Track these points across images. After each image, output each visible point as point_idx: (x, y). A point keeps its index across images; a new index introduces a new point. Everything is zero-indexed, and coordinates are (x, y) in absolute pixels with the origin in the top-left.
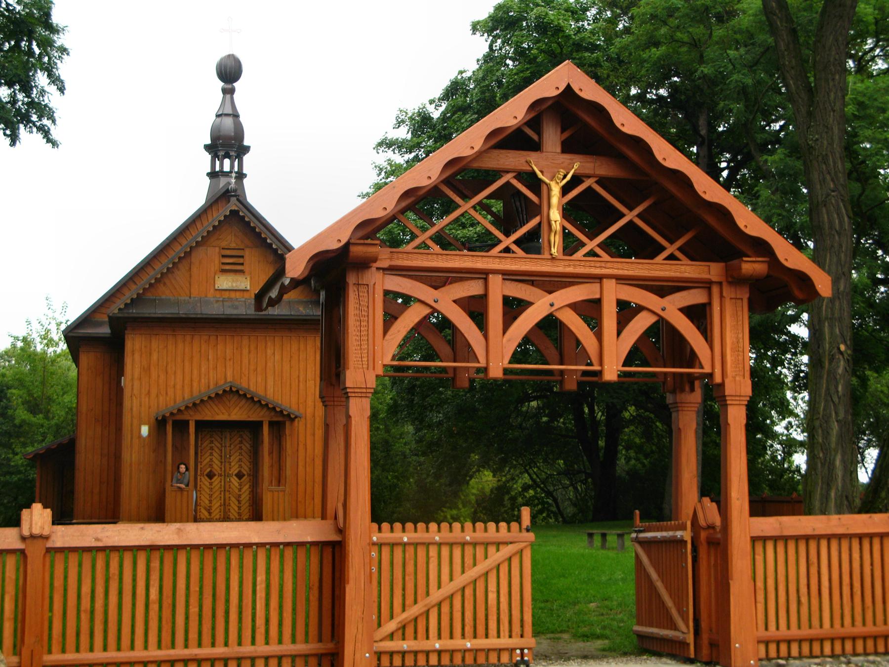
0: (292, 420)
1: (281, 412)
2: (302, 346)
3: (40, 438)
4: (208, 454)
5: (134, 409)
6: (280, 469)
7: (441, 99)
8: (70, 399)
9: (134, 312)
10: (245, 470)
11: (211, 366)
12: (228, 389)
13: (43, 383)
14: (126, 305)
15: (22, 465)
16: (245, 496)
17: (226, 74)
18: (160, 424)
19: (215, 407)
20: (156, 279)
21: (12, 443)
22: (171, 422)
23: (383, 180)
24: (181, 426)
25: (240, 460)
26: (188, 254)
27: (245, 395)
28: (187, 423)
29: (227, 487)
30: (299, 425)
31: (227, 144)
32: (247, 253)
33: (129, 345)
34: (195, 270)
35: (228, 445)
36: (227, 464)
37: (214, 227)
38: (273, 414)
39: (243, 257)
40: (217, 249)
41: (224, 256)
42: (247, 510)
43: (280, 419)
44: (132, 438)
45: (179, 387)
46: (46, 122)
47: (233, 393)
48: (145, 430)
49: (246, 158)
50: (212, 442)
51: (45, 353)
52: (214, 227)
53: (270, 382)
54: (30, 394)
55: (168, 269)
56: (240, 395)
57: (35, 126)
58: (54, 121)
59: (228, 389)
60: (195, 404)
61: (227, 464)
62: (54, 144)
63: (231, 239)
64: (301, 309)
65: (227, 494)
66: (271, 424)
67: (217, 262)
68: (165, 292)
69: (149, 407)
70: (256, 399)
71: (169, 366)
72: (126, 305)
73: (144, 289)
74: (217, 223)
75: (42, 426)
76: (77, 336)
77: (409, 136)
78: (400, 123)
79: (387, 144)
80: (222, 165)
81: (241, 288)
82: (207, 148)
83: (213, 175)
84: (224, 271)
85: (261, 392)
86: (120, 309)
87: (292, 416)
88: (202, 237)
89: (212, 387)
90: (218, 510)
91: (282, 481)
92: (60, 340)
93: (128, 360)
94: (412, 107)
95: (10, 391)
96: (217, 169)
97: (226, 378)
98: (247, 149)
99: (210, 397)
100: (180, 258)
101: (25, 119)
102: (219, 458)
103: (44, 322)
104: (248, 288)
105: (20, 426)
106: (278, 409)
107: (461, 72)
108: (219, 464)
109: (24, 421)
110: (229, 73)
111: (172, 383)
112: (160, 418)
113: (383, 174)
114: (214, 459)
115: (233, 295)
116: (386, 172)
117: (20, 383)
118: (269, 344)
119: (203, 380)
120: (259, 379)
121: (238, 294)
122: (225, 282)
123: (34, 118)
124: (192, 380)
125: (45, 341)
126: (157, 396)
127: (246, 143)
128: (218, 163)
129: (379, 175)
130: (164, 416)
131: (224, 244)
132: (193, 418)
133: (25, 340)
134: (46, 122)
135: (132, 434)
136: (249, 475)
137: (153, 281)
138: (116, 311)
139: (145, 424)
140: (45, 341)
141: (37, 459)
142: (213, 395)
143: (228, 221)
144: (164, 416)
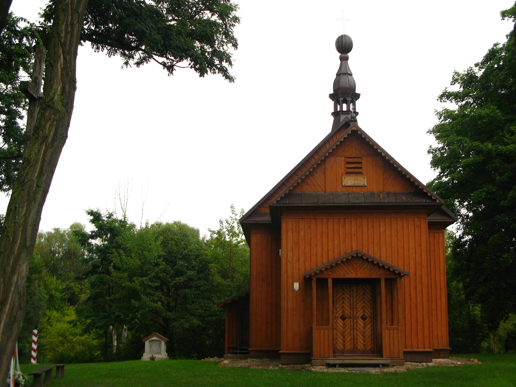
0: (401, 277)
1: (394, 271)
2: (405, 224)
3: (229, 294)
4: (341, 302)
5: (289, 271)
6: (392, 313)
7: (483, 63)
8: (245, 269)
9: (287, 203)
10: (368, 314)
11: (341, 240)
12: (355, 255)
13: (230, 259)
14: (282, 198)
15: (218, 311)
16: (368, 333)
17: (342, 47)
18: (307, 281)
19: (345, 268)
20: (302, 179)
21: (212, 297)
22: (315, 280)
23: (443, 122)
24: (322, 283)
25: (364, 307)
26: (323, 162)
27: (367, 259)
28: (326, 280)
29: (335, 326)
30: (405, 281)
31: (344, 92)
32: (364, 160)
33: (284, 226)
34: (328, 173)
35: (355, 296)
36: (355, 310)
37: (341, 142)
38: (387, 273)
39: (361, 163)
40: (343, 158)
41: (348, 163)
42: (370, 343)
43: (393, 277)
44: (287, 292)
45: (319, 255)
46: (225, 64)
47: (357, 258)
48: (296, 286)
49: (358, 102)
50: (343, 294)
51: (231, 241)
52: (341, 142)
53: (383, 249)
54: (222, 267)
55: (310, 172)
56: (364, 260)
57: (217, 68)
58: (230, 64)
59: (355, 255)
60: (332, 267)
61: (355, 310)
62: (231, 79)
63: (353, 150)
64: (404, 198)
65: (355, 331)
66: (387, 280)
67: (343, 167)
68: (308, 189)
69: (299, 270)
70: (375, 262)
71: (312, 240)
72: (282, 198)
73: (294, 187)
74: (342, 140)
75: (230, 286)
76: (249, 222)
77: (462, 89)
78: (454, 81)
79: (446, 96)
80: (341, 107)
81: (360, 185)
82: (332, 96)
83: (336, 114)
84: (348, 173)
85: (377, 256)
86: (277, 201)
87: (402, 274)
88: (333, 149)
89: (342, 254)
90: (349, 343)
91: (395, 322)
92: (240, 232)
93: (284, 237)
94: (462, 70)
95: (210, 265)
96: (339, 110)
97: (352, 249)
98: (358, 96)
99: (342, 262)
100: (318, 165)
101: (211, 65)
102: (349, 305)
103: (230, 220)
104: (366, 184)
105: (217, 286)
106: (391, 270)
107: (495, 45)
108: (349, 309)
109: (219, 283)
110: (344, 46)
111: (315, 252)
112: (307, 277)
113: (443, 118)
114: (346, 307)
115: (355, 190)
116: (444, 117)
117: (216, 259)
118: (382, 224)
119: (336, 250)
120: (376, 249)
121: (358, 189)
122: (349, 181)
123: (217, 62)
124: (328, 250)
125: (231, 234)
126: (304, 262)
127: (357, 91)
128: (339, 106)
129: (440, 119)
130: (310, 275)
131: (348, 154)
132: (330, 276)
133: (219, 233)
134: (225, 64)
135: (287, 289)
136: (370, 317)
137: (299, 181)
138: (275, 202)
139: (296, 282)
140: (231, 234)
141: (225, 306)
142: (345, 260)
143: (348, 142)
144: (310, 275)
